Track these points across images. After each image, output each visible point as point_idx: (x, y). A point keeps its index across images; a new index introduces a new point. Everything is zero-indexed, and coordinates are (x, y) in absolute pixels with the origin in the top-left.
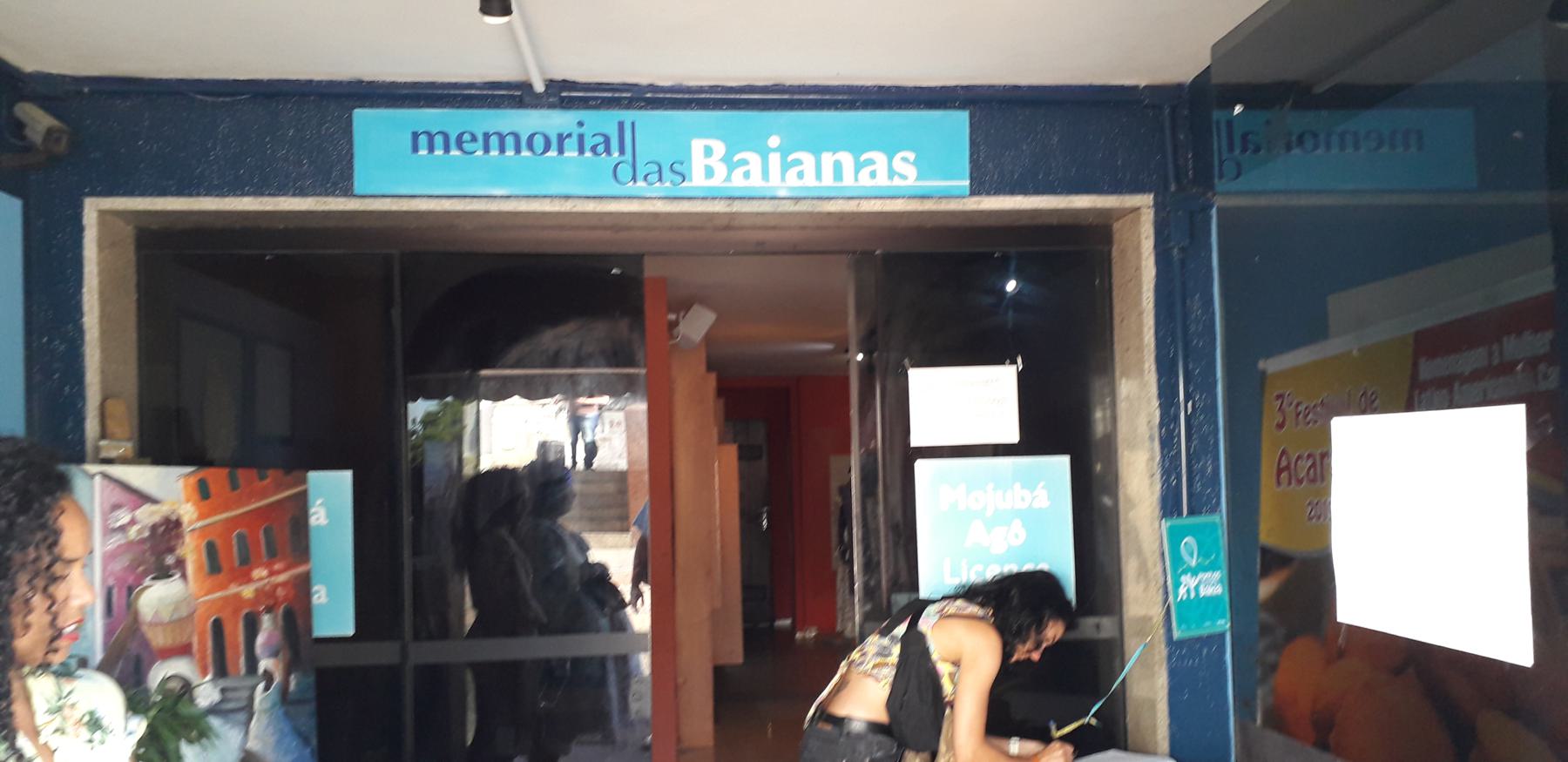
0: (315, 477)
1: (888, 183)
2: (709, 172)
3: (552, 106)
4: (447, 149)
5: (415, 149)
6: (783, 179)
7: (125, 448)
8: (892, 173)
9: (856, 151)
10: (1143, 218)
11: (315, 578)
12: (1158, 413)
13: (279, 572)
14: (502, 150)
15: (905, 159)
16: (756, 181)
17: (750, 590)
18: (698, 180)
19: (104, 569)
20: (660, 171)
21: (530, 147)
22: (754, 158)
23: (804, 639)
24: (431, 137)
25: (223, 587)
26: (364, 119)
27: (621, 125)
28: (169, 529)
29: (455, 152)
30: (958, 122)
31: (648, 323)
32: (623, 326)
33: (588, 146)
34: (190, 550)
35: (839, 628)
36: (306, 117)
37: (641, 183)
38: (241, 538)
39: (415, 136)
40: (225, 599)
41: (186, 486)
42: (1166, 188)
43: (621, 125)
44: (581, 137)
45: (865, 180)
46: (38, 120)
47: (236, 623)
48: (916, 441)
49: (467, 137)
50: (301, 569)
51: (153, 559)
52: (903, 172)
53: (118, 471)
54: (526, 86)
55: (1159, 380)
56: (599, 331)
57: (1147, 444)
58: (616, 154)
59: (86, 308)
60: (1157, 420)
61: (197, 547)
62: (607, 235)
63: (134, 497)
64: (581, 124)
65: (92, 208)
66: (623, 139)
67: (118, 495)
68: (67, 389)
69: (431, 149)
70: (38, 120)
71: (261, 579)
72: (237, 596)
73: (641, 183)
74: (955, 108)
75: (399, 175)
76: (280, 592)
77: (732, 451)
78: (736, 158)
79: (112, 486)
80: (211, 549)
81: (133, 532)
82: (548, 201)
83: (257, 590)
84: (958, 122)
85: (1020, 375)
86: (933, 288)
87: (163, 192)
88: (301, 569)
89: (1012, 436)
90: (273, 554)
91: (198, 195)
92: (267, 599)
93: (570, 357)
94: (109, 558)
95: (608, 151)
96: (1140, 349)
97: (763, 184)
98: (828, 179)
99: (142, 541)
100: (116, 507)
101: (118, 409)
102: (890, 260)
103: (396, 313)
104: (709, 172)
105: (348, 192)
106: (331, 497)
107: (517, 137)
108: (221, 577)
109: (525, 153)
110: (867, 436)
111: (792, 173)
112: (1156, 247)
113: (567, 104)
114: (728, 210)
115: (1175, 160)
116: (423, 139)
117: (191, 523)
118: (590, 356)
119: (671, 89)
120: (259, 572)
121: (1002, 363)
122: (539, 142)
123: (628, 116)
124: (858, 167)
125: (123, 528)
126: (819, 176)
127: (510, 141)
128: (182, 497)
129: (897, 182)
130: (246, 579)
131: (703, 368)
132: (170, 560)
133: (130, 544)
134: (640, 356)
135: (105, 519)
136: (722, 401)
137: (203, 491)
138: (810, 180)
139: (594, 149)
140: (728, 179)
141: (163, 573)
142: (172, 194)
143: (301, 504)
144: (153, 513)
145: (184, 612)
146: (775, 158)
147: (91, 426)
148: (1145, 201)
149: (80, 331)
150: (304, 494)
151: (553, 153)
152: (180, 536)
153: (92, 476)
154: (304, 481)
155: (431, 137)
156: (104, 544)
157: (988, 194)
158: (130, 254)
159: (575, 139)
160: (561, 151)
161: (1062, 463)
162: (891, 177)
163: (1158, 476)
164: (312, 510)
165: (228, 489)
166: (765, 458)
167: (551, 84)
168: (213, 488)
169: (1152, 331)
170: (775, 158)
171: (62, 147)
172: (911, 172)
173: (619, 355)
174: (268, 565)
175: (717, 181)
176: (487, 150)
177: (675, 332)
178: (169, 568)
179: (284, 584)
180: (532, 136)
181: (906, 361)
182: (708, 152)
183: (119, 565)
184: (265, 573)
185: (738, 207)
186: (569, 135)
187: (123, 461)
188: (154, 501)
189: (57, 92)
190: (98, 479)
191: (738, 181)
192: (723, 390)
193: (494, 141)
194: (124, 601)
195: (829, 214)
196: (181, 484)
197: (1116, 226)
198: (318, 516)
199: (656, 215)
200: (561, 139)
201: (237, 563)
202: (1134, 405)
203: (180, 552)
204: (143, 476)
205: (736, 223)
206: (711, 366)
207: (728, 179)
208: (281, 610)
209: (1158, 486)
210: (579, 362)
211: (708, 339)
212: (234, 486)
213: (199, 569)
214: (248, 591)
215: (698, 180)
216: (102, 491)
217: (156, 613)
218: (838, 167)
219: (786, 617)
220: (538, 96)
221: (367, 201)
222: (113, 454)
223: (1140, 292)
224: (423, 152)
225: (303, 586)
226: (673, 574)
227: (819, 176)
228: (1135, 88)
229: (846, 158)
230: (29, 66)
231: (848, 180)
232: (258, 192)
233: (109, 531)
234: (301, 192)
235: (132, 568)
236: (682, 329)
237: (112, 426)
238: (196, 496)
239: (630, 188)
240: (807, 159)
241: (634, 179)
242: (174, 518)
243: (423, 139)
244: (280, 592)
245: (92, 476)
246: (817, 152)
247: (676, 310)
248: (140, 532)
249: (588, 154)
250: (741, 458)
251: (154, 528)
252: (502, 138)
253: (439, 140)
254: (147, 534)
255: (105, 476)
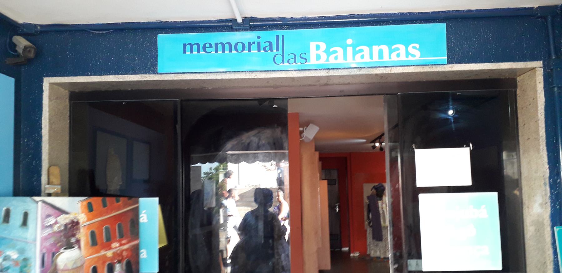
0: (142, 200)
1: (405, 59)
2: (318, 57)
3: (246, 30)
4: (199, 51)
5: (185, 52)
6: (354, 59)
7: (57, 188)
8: (408, 54)
9: (390, 44)
10: (538, 73)
11: (141, 246)
12: (548, 171)
13: (124, 244)
14: (223, 51)
15: (414, 47)
16: (340, 61)
17: (333, 236)
18: (313, 61)
19: (41, 245)
20: (295, 58)
21: (236, 49)
22: (340, 50)
23: (354, 256)
24: (192, 46)
25: (98, 252)
26: (162, 38)
27: (277, 37)
28: (74, 225)
29: (202, 52)
30: (442, 27)
31: (289, 131)
32: (278, 131)
33: (262, 48)
34: (83, 235)
35: (368, 253)
36: (137, 39)
37: (286, 64)
38: (106, 228)
39: (185, 45)
40: (99, 258)
41: (82, 205)
42: (550, 56)
43: (277, 37)
44: (259, 43)
45: (394, 57)
46: (21, 42)
47: (104, 268)
48: (420, 183)
49: (208, 45)
50: (135, 242)
51: (65, 240)
52: (414, 50)
53: (50, 200)
54: (234, 21)
55: (548, 155)
56: (267, 134)
57: (543, 186)
58: (275, 51)
59: (43, 126)
60: (548, 175)
61: (86, 234)
62: (272, 89)
63: (57, 211)
64: (259, 37)
65: (47, 82)
66: (278, 44)
67: (50, 211)
68: (34, 162)
69: (192, 52)
70: (21, 42)
71: (116, 247)
72: (104, 256)
73: (286, 64)
74: (439, 22)
75: (178, 65)
76: (125, 254)
77: (325, 182)
78: (331, 50)
79: (47, 206)
80: (93, 234)
81: (56, 228)
82: (244, 73)
83: (114, 253)
84: (442, 27)
85: (471, 151)
86: (421, 111)
87: (76, 75)
88: (135, 242)
89: (468, 182)
90: (122, 236)
91: (91, 75)
92: (119, 257)
93: (255, 145)
94: (44, 239)
95: (271, 50)
96: (537, 139)
97: (344, 62)
98: (376, 58)
99: (61, 231)
100: (49, 216)
101: (56, 171)
102: (404, 98)
103: (178, 127)
104: (318, 57)
105: (155, 72)
106: (150, 210)
107: (230, 44)
108: (97, 247)
109: (234, 52)
110: (394, 181)
111: (358, 56)
112: (544, 87)
113: (253, 28)
114: (327, 75)
115: (554, 43)
116: (188, 47)
117: (83, 223)
118: (264, 145)
119: (300, 19)
120: (115, 245)
121: (462, 146)
122: (240, 47)
123: (280, 32)
124: (391, 52)
125: (51, 226)
126: (371, 57)
127: (227, 46)
128: (80, 211)
129: (410, 58)
130: (109, 248)
131: (314, 149)
132: (73, 240)
133: (55, 233)
134: (286, 145)
135: (43, 222)
136: (321, 162)
137: (90, 208)
138: (367, 59)
139: (265, 49)
140: (327, 60)
141: (69, 246)
142: (80, 75)
143: (136, 212)
144: (66, 218)
145: (79, 265)
146: (350, 50)
147: (44, 178)
148: (538, 64)
149: (41, 136)
150: (137, 208)
151: (246, 51)
152: (78, 229)
153: (37, 202)
154: (137, 202)
155: (192, 46)
156: (42, 233)
157: (456, 63)
158: (67, 103)
159: (256, 44)
160: (250, 50)
161: (494, 195)
162: (407, 56)
163: (549, 204)
164: (141, 216)
165: (102, 207)
166: (337, 185)
167: (245, 19)
168: (94, 207)
169: (544, 130)
170: (350, 50)
171: (32, 55)
172: (417, 53)
173: (277, 145)
174: (119, 241)
175: (322, 61)
176: (216, 51)
177: (302, 135)
178: (72, 243)
179: (126, 250)
180: (236, 44)
181: (414, 146)
182: (318, 47)
183: (47, 244)
184: (118, 245)
185: (332, 73)
186: (254, 43)
187: (57, 195)
188: (67, 213)
189: (31, 32)
190: (40, 203)
191: (332, 61)
192: (321, 159)
193: (220, 46)
194: (50, 260)
195: (376, 75)
196: (79, 205)
197: (518, 79)
198: (143, 218)
199: (293, 79)
200: (250, 44)
201: (105, 241)
202: (531, 165)
203: (77, 236)
204: (62, 202)
205: (330, 82)
206: (316, 150)
207: (327, 60)
208: (125, 262)
209: (549, 209)
210: (258, 148)
211: (315, 138)
212: (105, 205)
213: (87, 243)
214: (109, 254)
215: (313, 61)
216: (42, 209)
217: (65, 265)
218: (381, 53)
219: (346, 247)
220: (239, 24)
221: (163, 75)
222: (52, 191)
223: (537, 110)
224: (188, 53)
225: (136, 250)
226: (302, 234)
227: (371, 57)
228: (532, 8)
229: (385, 48)
230: (20, 20)
231: (386, 58)
232: (116, 73)
233: (44, 227)
234: (135, 73)
235: (55, 244)
236: (305, 134)
237: (53, 179)
238: (87, 211)
239: (281, 66)
240: (366, 49)
241: (283, 62)
242: (76, 220)
243: (188, 47)
244: (125, 254)
245: (37, 202)
246: (370, 46)
247: (303, 127)
248: (59, 227)
249: (262, 51)
250: (328, 184)
251: (66, 225)
252: (223, 45)
253: (195, 47)
254: (62, 228)
255: (44, 202)
